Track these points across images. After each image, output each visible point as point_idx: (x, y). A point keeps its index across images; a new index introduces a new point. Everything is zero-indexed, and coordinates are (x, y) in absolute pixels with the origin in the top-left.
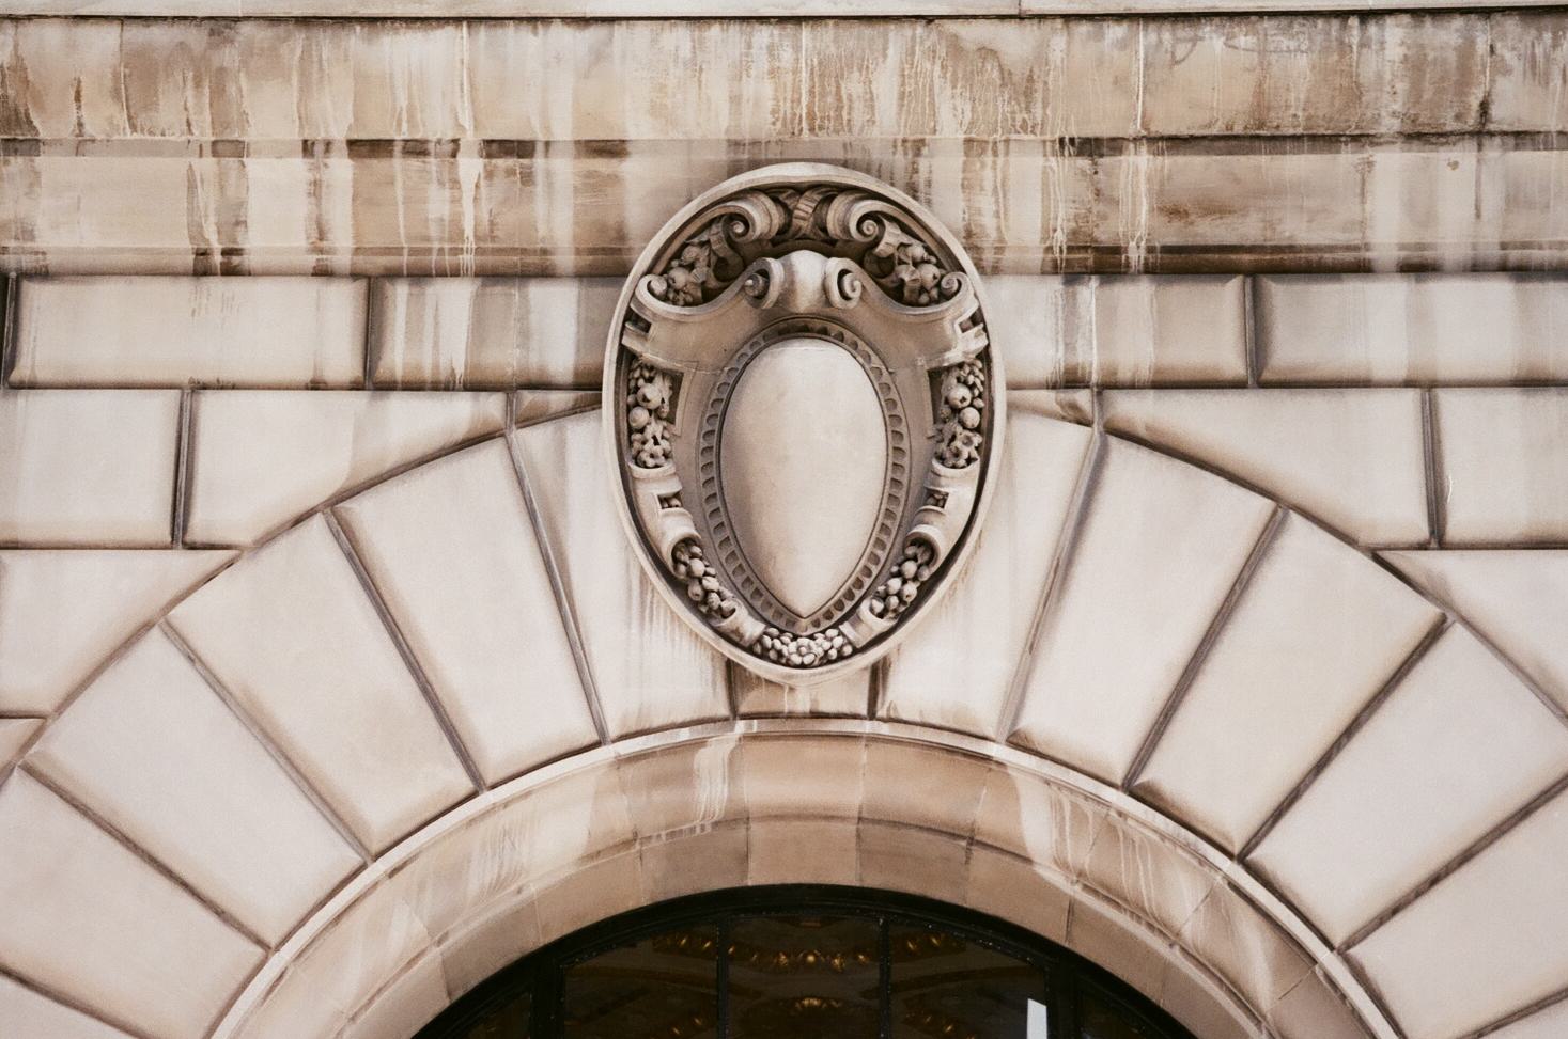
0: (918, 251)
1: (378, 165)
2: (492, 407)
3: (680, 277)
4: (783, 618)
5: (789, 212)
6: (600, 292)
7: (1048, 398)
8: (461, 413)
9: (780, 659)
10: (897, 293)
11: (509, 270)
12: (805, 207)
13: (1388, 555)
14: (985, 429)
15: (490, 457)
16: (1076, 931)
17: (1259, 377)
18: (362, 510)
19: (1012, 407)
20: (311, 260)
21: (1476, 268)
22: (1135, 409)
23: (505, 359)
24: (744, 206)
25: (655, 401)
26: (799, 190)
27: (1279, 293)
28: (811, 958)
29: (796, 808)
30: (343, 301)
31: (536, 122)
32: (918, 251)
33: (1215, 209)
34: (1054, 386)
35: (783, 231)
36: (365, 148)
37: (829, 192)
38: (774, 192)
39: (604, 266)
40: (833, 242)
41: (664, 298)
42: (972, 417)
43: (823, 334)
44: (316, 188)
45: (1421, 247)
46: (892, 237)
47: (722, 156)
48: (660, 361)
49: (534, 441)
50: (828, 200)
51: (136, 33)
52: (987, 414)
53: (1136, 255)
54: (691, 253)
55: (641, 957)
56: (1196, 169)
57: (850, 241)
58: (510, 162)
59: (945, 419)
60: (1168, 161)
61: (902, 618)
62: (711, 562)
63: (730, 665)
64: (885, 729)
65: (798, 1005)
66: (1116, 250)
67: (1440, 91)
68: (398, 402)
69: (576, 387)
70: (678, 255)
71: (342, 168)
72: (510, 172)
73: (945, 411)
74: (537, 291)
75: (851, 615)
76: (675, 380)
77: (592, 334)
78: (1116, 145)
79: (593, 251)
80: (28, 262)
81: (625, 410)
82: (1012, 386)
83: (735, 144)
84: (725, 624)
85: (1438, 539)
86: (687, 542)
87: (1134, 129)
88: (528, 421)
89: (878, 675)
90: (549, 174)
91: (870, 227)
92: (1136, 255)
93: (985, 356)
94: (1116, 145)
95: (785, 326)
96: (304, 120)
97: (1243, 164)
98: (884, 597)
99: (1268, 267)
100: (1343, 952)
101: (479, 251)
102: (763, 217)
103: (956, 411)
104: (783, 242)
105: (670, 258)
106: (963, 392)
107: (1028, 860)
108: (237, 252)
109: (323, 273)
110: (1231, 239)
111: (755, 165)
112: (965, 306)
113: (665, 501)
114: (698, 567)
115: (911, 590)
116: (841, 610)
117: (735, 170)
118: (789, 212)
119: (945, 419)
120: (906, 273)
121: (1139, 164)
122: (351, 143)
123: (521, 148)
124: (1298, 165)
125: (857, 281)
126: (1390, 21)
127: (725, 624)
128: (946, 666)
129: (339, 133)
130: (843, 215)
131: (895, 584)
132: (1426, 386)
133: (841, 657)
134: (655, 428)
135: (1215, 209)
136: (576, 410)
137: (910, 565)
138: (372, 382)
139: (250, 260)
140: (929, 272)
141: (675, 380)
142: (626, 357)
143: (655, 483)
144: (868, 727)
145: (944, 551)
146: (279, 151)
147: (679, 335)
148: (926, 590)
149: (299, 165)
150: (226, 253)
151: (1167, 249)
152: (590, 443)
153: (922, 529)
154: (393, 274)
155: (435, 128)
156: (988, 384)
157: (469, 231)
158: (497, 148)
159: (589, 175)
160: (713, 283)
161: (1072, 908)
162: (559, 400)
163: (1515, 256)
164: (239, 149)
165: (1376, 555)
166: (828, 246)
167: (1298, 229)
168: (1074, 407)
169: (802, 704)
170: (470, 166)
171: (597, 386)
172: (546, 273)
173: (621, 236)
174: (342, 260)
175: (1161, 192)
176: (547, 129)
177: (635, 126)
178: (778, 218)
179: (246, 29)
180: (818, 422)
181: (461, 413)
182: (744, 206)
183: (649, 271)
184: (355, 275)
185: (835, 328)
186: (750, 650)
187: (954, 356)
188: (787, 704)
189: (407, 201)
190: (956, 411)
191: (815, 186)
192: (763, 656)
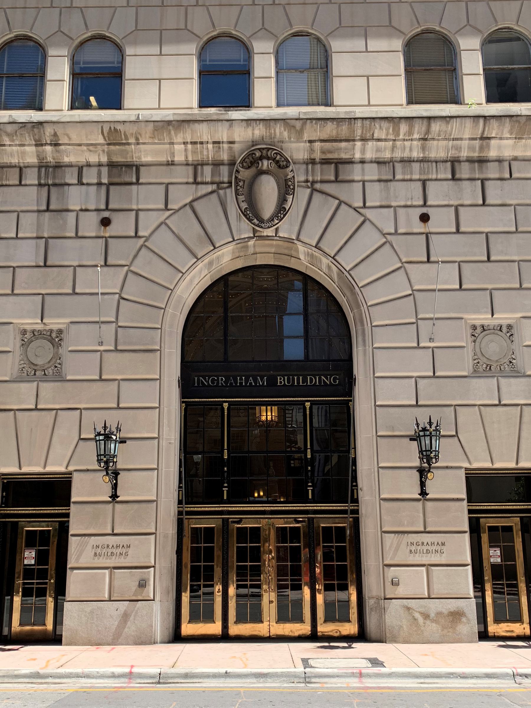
0: (283, 159)
1: (195, 146)
2: (214, 187)
3: (245, 164)
4: (261, 221)
5: (262, 153)
6: (232, 167)
7: (303, 184)
8: (210, 188)
9: (262, 227)
10: (279, 167)
11: (217, 164)
12: (264, 152)
13: (358, 209)
14: (294, 189)
15: (215, 195)
16: (307, 270)
17: (336, 181)
18: (195, 204)
19: (298, 186)
20: (185, 162)
21: (371, 162)
22: (318, 186)
23: (217, 179)
24: (255, 152)
25: (241, 185)
26: (263, 149)
27: (340, 166)
28: (268, 414)
29: (264, 255)
30: (191, 169)
31: (220, 138)
32: (283, 159)
33: (330, 152)
34: (304, 182)
35: (261, 156)
36: (194, 143)
37: (269, 149)
38: (259, 149)
39: (232, 164)
40: (269, 158)
41: (242, 168)
42: (292, 187)
43: (267, 173)
44: (186, 150)
45: (362, 158)
46: (278, 157)
47: (251, 143)
48: (241, 178)
49: (221, 192)
50: (268, 151)
51: (156, 124)
52: (294, 186)
53: (318, 160)
54: (247, 160)
55: (239, 277)
56: (328, 145)
57: (272, 158)
58: (217, 145)
59: (286, 189)
60: (323, 144)
61: (281, 220)
62: (252, 212)
63: (253, 228)
64: (278, 238)
65: (262, 494)
66: (315, 159)
67: (366, 132)
68: (200, 186)
69: (228, 183)
70: (244, 160)
71: (189, 146)
72: (217, 147)
73: (287, 186)
74: (221, 167)
75: (273, 220)
76: (244, 181)
77: (230, 176)
78: (314, 141)
79: (231, 160)
80: (141, 163)
81: (236, 187)
82: (298, 182)
83: (253, 142)
84: (253, 222)
85: (364, 206)
86: (246, 208)
87: (317, 139)
88: (221, 189)
89: (277, 230)
90: (223, 147)
91: (275, 155)
92: (318, 160)
93: (294, 177)
94: (314, 141)
95: (262, 172)
96: (184, 138)
97: (335, 144)
98: (278, 217)
99: (339, 163)
100: (348, 272)
101: (212, 160)
102: (258, 154)
103: (289, 186)
104: (261, 158)
105: (243, 161)
106: (290, 183)
107: (300, 259)
108: (174, 161)
109: (187, 165)
110: (332, 157)
111: (256, 145)
112: (291, 168)
113: (243, 201)
114: (248, 212)
115: (282, 216)
116: (271, 219)
117: (253, 146)
118: (262, 153)
119: (286, 189)
120: (281, 163)
121: (317, 145)
122: (191, 142)
123: (219, 143)
124: (343, 145)
125: (273, 165)
126: (359, 120)
127: (253, 222)
128: (287, 228)
129: (189, 141)
130: (271, 154)
131: (279, 215)
132: (364, 182)
133: (271, 227)
134: (241, 190)
135: (330, 152)
136: (228, 187)
137: (281, 211)
138: (196, 183)
139: (176, 163)
140: (285, 163)
141: (244, 181)
142: (236, 178)
143: (241, 198)
144: (275, 238)
145: (287, 210)
146: (179, 143)
147: (245, 174)
148: (284, 216)
149: (183, 146)
150: (172, 161)
151: (323, 159)
152: (230, 194)
153: (284, 206)
154: (198, 165)
155: (205, 139)
156: (294, 181)
157: (210, 159)
158: (214, 143)
159: (229, 147)
160: (250, 165)
161: (307, 266)
162: (225, 185)
163: (377, 160)
164: (173, 143)
165: (355, 209)
166: (268, 159)
167: (344, 156)
168: (308, 185)
169: (265, 234)
170: (210, 146)
171: (231, 183)
172: (223, 164)
173: (235, 158)
174: (190, 162)
175: (322, 149)
176: (222, 139)
177: (237, 139)
178: (260, 154)
179: (173, 122)
180: (268, 190)
181: (210, 188)
182: (255, 152)
183: (240, 163)
184: (192, 165)
185: (270, 172)
186: (257, 226)
187: (289, 177)
188: (262, 234)
189: (200, 152)
190: (289, 186)
191: (266, 148)
192: (259, 227)
